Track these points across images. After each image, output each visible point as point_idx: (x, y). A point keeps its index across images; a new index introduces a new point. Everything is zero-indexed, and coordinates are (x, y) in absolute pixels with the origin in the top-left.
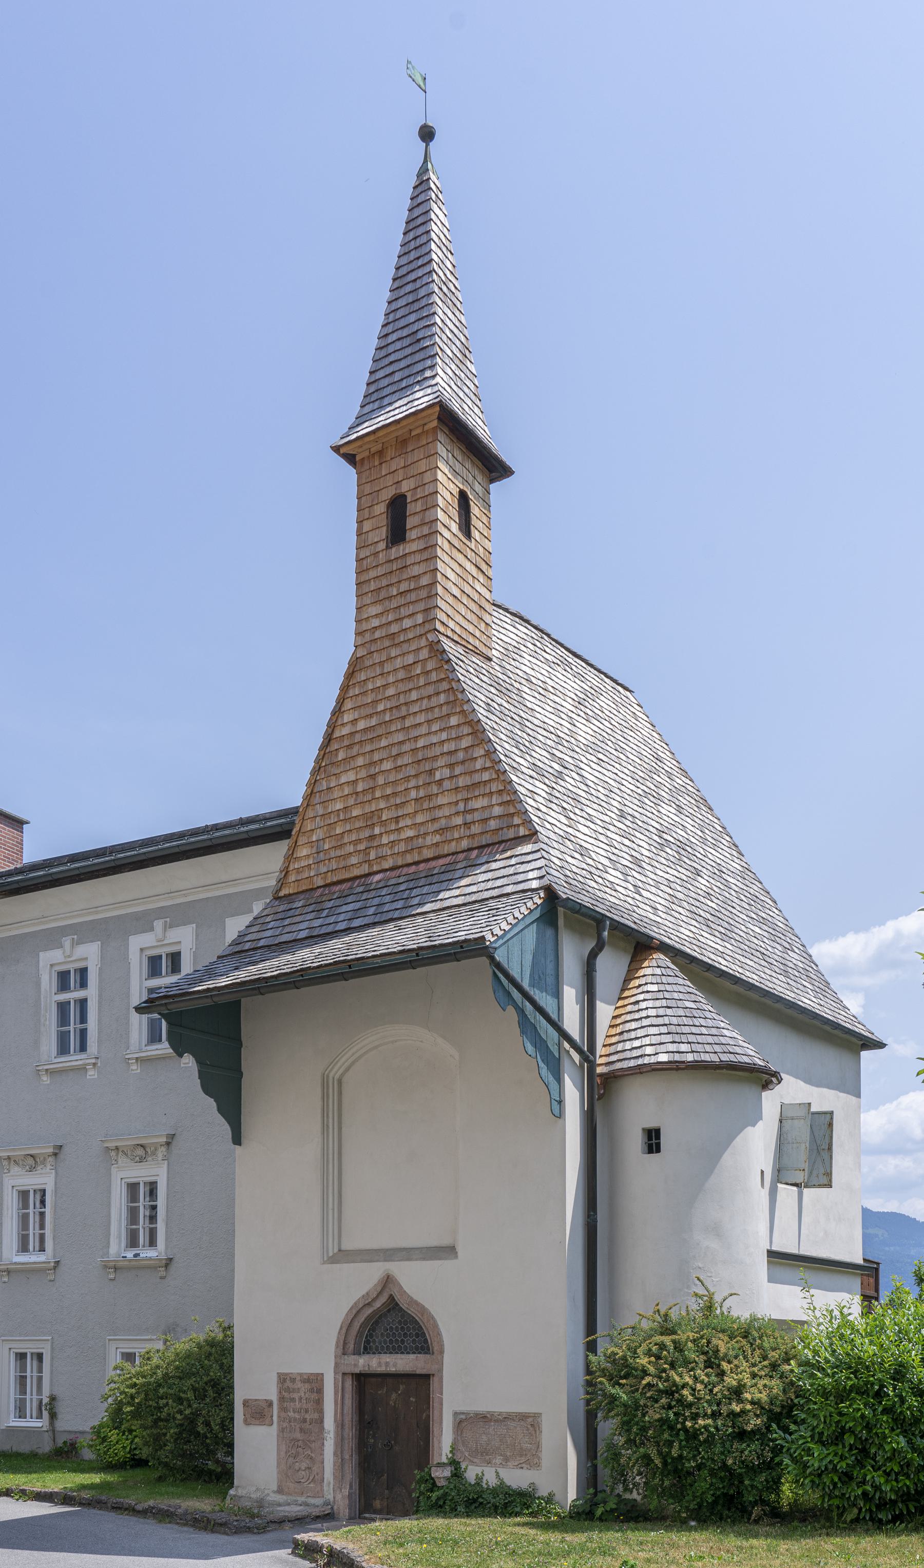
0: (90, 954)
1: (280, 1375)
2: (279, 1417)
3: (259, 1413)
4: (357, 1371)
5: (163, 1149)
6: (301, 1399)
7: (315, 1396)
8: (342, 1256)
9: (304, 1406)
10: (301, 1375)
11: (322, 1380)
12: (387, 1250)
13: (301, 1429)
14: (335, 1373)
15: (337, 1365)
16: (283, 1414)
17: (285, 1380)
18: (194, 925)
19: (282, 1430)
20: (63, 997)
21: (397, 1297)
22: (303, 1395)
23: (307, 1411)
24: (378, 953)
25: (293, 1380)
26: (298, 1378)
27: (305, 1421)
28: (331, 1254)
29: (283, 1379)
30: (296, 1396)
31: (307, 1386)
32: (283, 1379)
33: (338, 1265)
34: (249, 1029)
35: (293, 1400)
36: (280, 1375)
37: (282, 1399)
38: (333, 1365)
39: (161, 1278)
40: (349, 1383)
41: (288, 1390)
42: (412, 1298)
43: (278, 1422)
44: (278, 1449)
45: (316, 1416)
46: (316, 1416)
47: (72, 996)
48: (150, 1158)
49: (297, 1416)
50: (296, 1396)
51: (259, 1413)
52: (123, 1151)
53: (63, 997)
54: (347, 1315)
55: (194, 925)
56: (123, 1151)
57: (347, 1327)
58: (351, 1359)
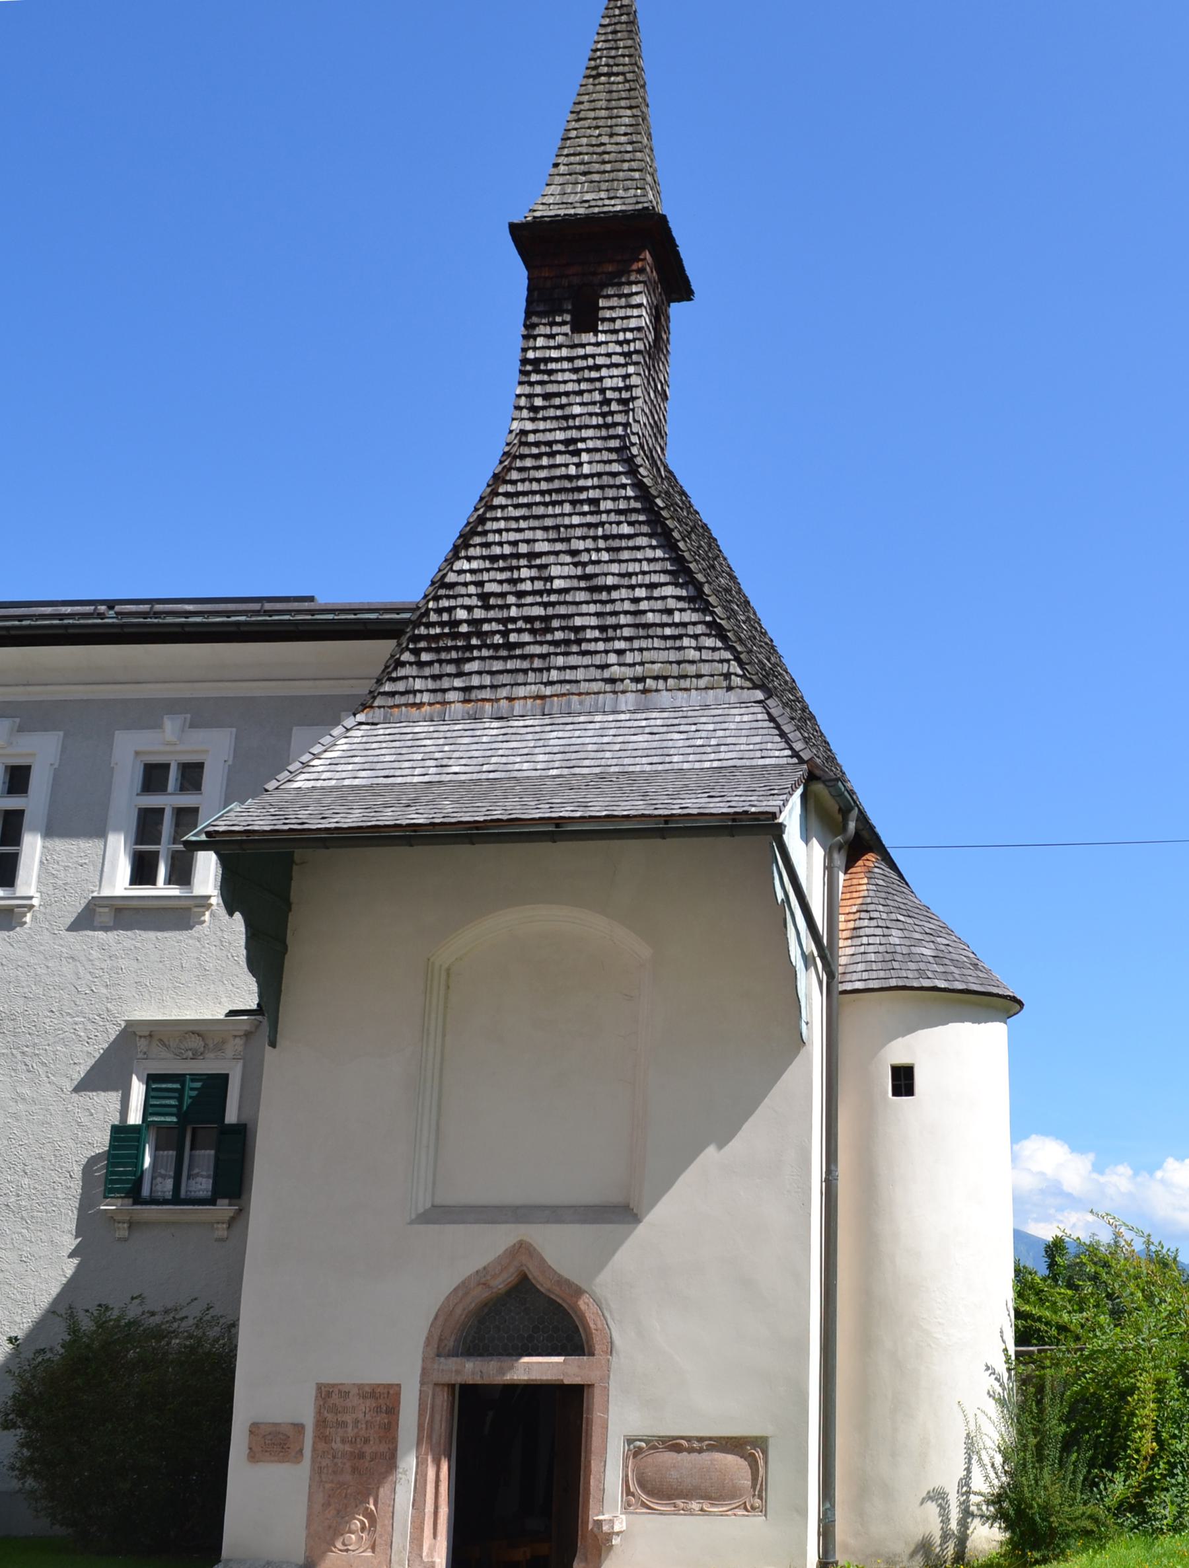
0: (215, 748)
1: (319, 1387)
2: (314, 1450)
3: (276, 1443)
4: (460, 1380)
5: (239, 1042)
6: (356, 1422)
7: (382, 1418)
8: (440, 1214)
9: (363, 1433)
10: (360, 1387)
11: (398, 1394)
12: (518, 1207)
13: (354, 1470)
14: (422, 1383)
15: (424, 1372)
16: (322, 1446)
17: (329, 1394)
18: (61, 733)
19: (317, 1470)
20: (153, 801)
21: (535, 1274)
22: (361, 1416)
23: (367, 1441)
24: (453, 820)
25: (345, 1394)
26: (354, 1391)
27: (361, 1455)
28: (421, 1210)
29: (325, 1393)
30: (348, 1418)
31: (371, 1403)
32: (325, 1393)
33: (436, 1227)
34: (300, 887)
35: (344, 1424)
36: (319, 1387)
37: (321, 1423)
38: (419, 1372)
39: (221, 1240)
40: (443, 1398)
41: (334, 1410)
42: (559, 1276)
43: (313, 1460)
44: (310, 1500)
45: (383, 1448)
46: (383, 1448)
47: (169, 801)
48: (212, 1055)
49: (348, 1448)
50: (348, 1418)
51: (276, 1443)
52: (161, 1040)
53: (153, 801)
54: (448, 1298)
55: (61, 733)
56: (161, 1040)
57: (443, 1315)
58: (453, 1363)
